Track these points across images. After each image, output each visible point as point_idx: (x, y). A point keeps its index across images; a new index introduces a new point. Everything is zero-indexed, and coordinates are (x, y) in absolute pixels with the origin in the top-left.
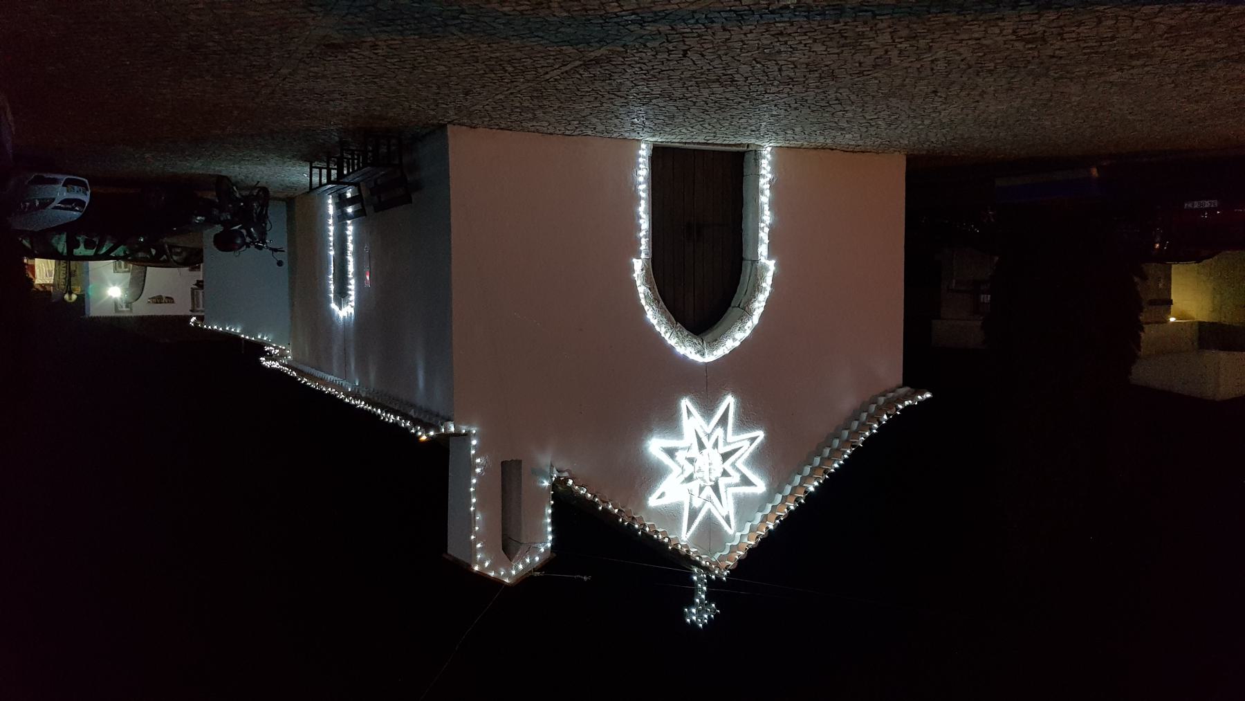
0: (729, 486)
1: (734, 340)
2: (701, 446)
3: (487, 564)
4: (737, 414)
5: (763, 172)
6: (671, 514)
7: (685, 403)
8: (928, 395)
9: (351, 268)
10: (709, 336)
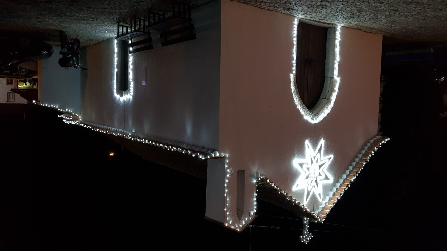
0: (321, 180)
1: (324, 113)
2: (312, 162)
3: (230, 222)
4: (325, 147)
5: (337, 37)
6: (300, 194)
7: (307, 143)
8: (389, 139)
9: (131, 77)
10: (315, 112)
